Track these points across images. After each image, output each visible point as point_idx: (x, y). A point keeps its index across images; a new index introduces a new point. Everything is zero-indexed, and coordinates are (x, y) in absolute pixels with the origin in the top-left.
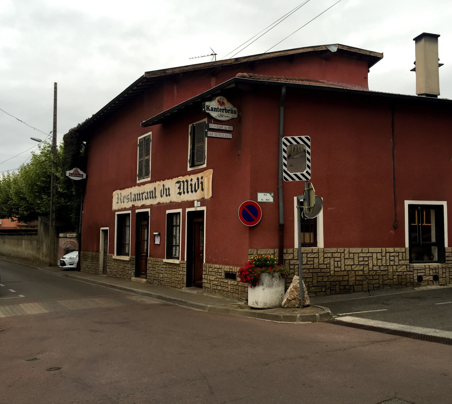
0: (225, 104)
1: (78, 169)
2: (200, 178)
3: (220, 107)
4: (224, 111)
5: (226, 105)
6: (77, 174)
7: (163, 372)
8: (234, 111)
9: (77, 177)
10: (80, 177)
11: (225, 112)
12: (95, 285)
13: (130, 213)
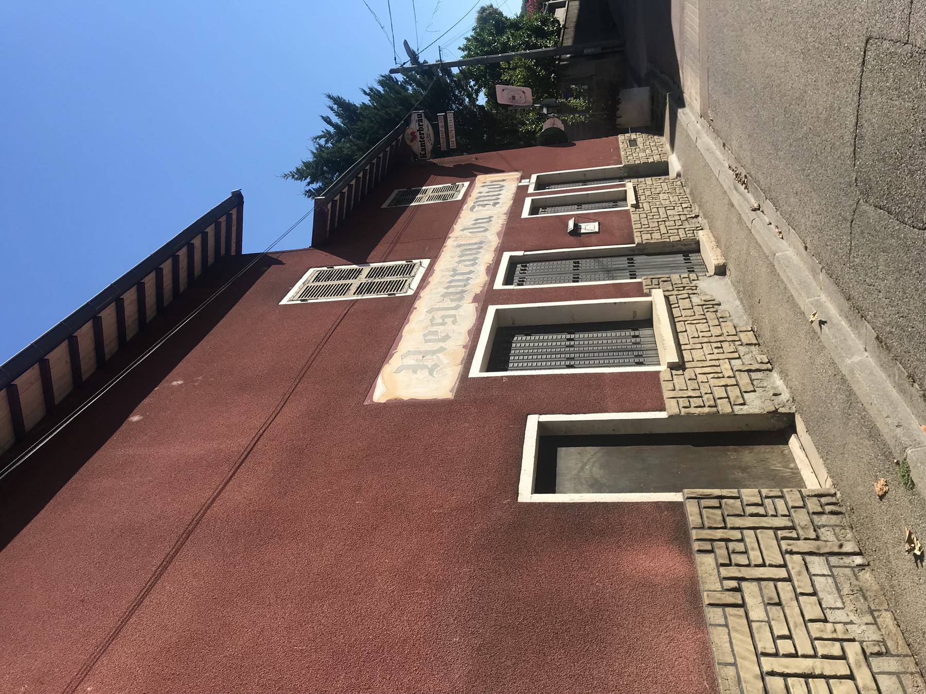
0: (412, 131)
2: (727, 334)
4: (422, 132)
5: (413, 129)
8: (418, 118)
11: (423, 130)
12: (565, 63)
13: (532, 200)
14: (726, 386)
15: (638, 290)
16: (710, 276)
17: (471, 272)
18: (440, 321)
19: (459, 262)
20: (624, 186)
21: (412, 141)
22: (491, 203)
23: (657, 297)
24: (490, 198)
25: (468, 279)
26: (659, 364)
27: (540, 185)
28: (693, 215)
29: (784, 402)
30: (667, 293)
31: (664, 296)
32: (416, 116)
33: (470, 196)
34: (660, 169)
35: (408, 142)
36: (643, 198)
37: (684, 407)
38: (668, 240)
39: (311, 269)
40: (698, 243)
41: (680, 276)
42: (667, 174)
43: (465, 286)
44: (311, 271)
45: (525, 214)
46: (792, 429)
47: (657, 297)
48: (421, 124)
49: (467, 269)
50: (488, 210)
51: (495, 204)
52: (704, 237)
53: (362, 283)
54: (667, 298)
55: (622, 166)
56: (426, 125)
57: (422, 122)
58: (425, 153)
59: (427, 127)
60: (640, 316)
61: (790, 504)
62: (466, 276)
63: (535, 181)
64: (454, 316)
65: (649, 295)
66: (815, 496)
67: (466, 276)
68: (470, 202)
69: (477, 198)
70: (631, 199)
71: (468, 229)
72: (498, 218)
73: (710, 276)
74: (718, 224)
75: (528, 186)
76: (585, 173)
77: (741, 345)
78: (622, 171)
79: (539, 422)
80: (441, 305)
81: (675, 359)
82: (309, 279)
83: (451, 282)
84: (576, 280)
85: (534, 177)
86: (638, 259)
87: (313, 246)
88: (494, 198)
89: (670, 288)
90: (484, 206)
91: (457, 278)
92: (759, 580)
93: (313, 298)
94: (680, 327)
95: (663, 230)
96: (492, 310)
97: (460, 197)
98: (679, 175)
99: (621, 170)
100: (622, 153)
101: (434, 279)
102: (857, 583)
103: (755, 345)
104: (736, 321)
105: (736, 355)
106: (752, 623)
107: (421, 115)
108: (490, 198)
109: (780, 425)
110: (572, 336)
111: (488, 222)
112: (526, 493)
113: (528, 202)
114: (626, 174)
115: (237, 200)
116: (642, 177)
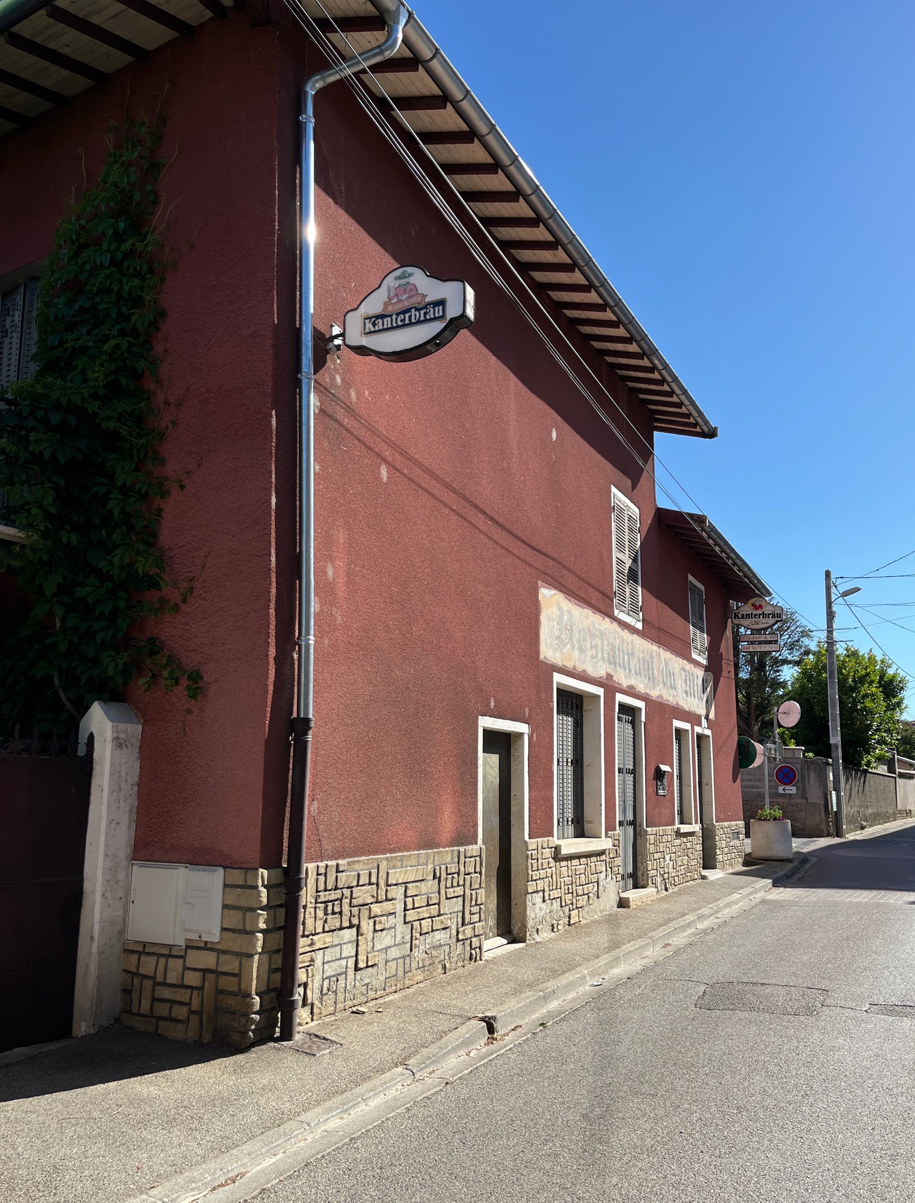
1: (410, 275)
3: (754, 612)
4: (761, 616)
5: (766, 606)
6: (408, 310)
7: (784, 906)
8: (777, 614)
9: (411, 324)
10: (426, 321)
11: (763, 617)
14: (544, 891)
15: (610, 827)
16: (619, 893)
17: (630, 670)
18: (594, 643)
19: (638, 658)
20: (696, 823)
21: (753, 605)
22: (688, 689)
23: (603, 843)
24: (692, 687)
25: (624, 667)
26: (558, 839)
27: (700, 737)
28: (668, 886)
29: (533, 938)
30: (607, 852)
31: (605, 850)
32: (778, 612)
33: (695, 667)
34: (709, 862)
35: (752, 601)
36: (685, 840)
37: (532, 854)
38: (648, 859)
39: (638, 510)
40: (644, 887)
41: (619, 866)
42: (704, 868)
43: (619, 665)
44: (637, 510)
45: (677, 724)
46: (512, 941)
47: (603, 843)
48: (770, 616)
49: (632, 667)
50: (681, 686)
51: (686, 692)
52: (650, 890)
53: (624, 563)
54: (602, 853)
55: (714, 823)
56: (768, 622)
57: (772, 617)
58: (738, 618)
59: (767, 623)
60: (587, 826)
61: (476, 925)
62: (627, 666)
63: (705, 733)
64: (597, 657)
65: (606, 836)
66: (480, 945)
67: (627, 666)
68: (689, 666)
69: (692, 674)
70: (685, 828)
71: (666, 666)
72: (674, 696)
73: (619, 893)
74: (665, 906)
75: (701, 726)
76: (709, 784)
77: (570, 910)
78: (709, 823)
79: (524, 733)
80: (606, 643)
81: (564, 852)
82: (631, 510)
83: (623, 651)
84: (620, 771)
85: (708, 732)
86: (630, 830)
87: (658, 508)
88: (692, 691)
89: (611, 856)
90: (686, 682)
91: (626, 657)
92: (439, 893)
93: (616, 517)
94: (583, 860)
95: (656, 856)
96: (599, 691)
97: (695, 656)
98: (704, 878)
99: (710, 821)
100: (726, 824)
101: (626, 634)
102: (437, 961)
103: (569, 922)
104: (586, 909)
105: (563, 904)
106: (274, 910)
107: (780, 617)
108: (692, 687)
109: (516, 928)
110: (569, 764)
111: (671, 686)
112: (486, 722)
113: (686, 726)
114: (705, 826)
115: (711, 434)
116: (702, 841)
